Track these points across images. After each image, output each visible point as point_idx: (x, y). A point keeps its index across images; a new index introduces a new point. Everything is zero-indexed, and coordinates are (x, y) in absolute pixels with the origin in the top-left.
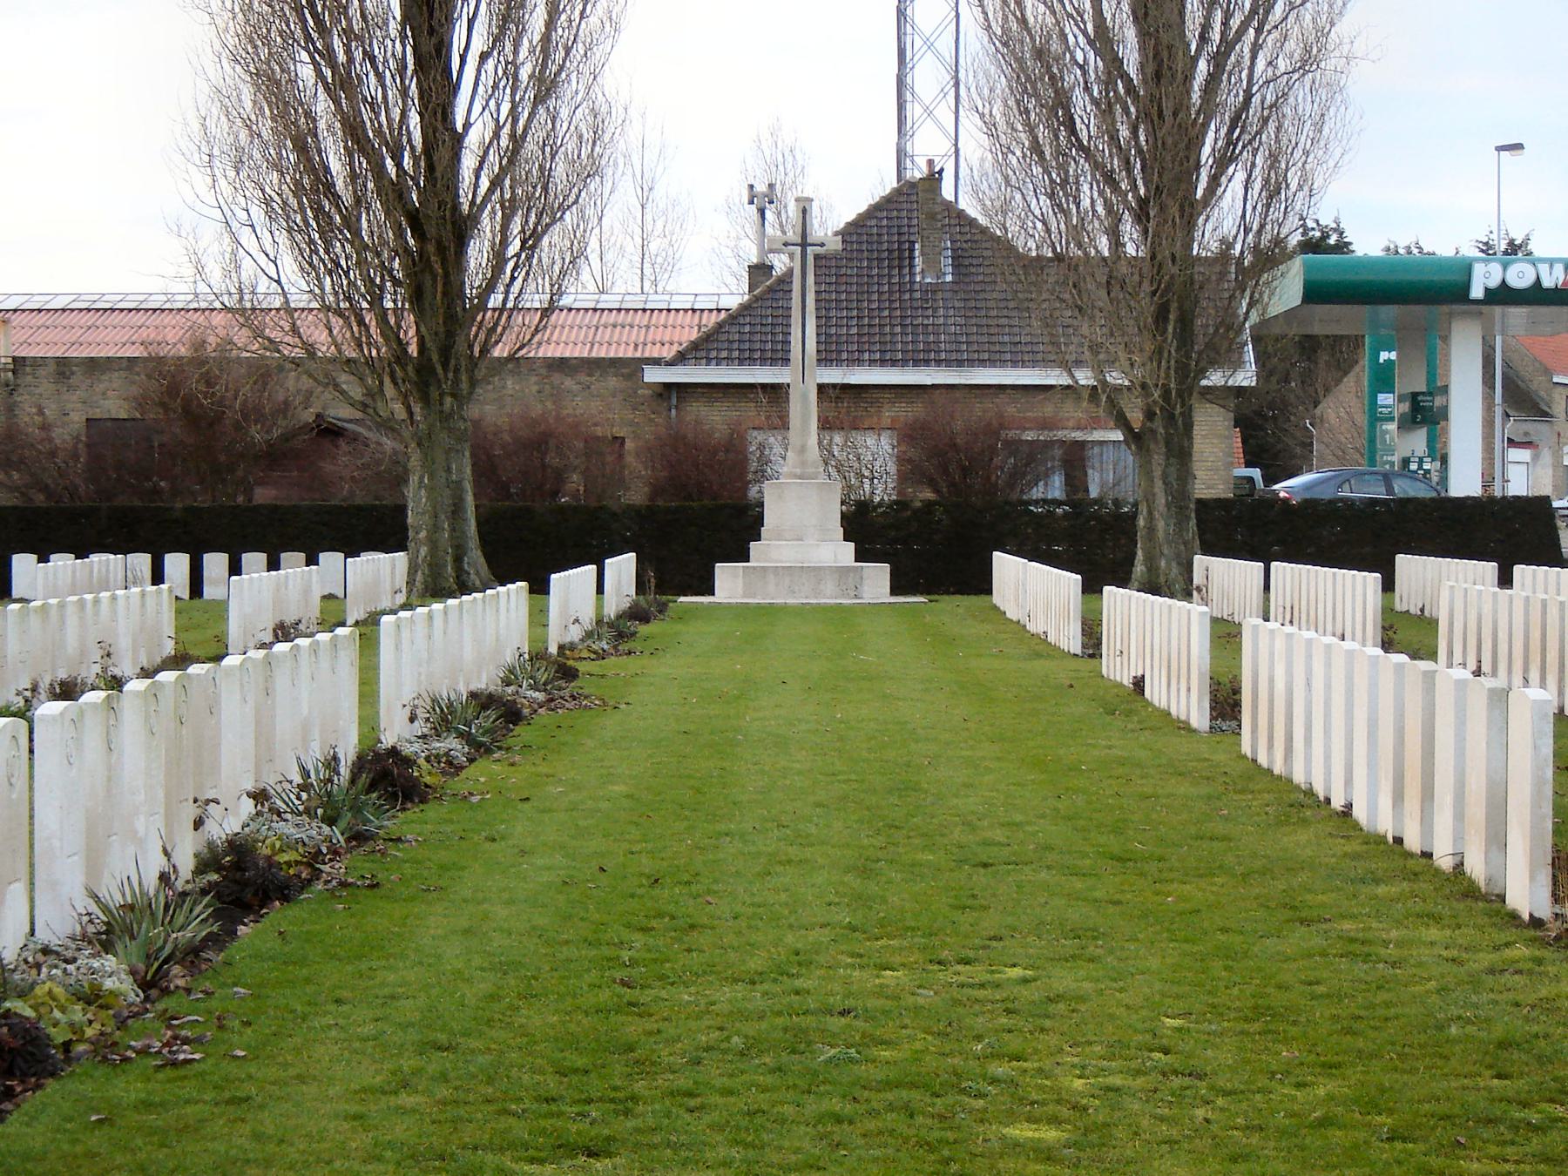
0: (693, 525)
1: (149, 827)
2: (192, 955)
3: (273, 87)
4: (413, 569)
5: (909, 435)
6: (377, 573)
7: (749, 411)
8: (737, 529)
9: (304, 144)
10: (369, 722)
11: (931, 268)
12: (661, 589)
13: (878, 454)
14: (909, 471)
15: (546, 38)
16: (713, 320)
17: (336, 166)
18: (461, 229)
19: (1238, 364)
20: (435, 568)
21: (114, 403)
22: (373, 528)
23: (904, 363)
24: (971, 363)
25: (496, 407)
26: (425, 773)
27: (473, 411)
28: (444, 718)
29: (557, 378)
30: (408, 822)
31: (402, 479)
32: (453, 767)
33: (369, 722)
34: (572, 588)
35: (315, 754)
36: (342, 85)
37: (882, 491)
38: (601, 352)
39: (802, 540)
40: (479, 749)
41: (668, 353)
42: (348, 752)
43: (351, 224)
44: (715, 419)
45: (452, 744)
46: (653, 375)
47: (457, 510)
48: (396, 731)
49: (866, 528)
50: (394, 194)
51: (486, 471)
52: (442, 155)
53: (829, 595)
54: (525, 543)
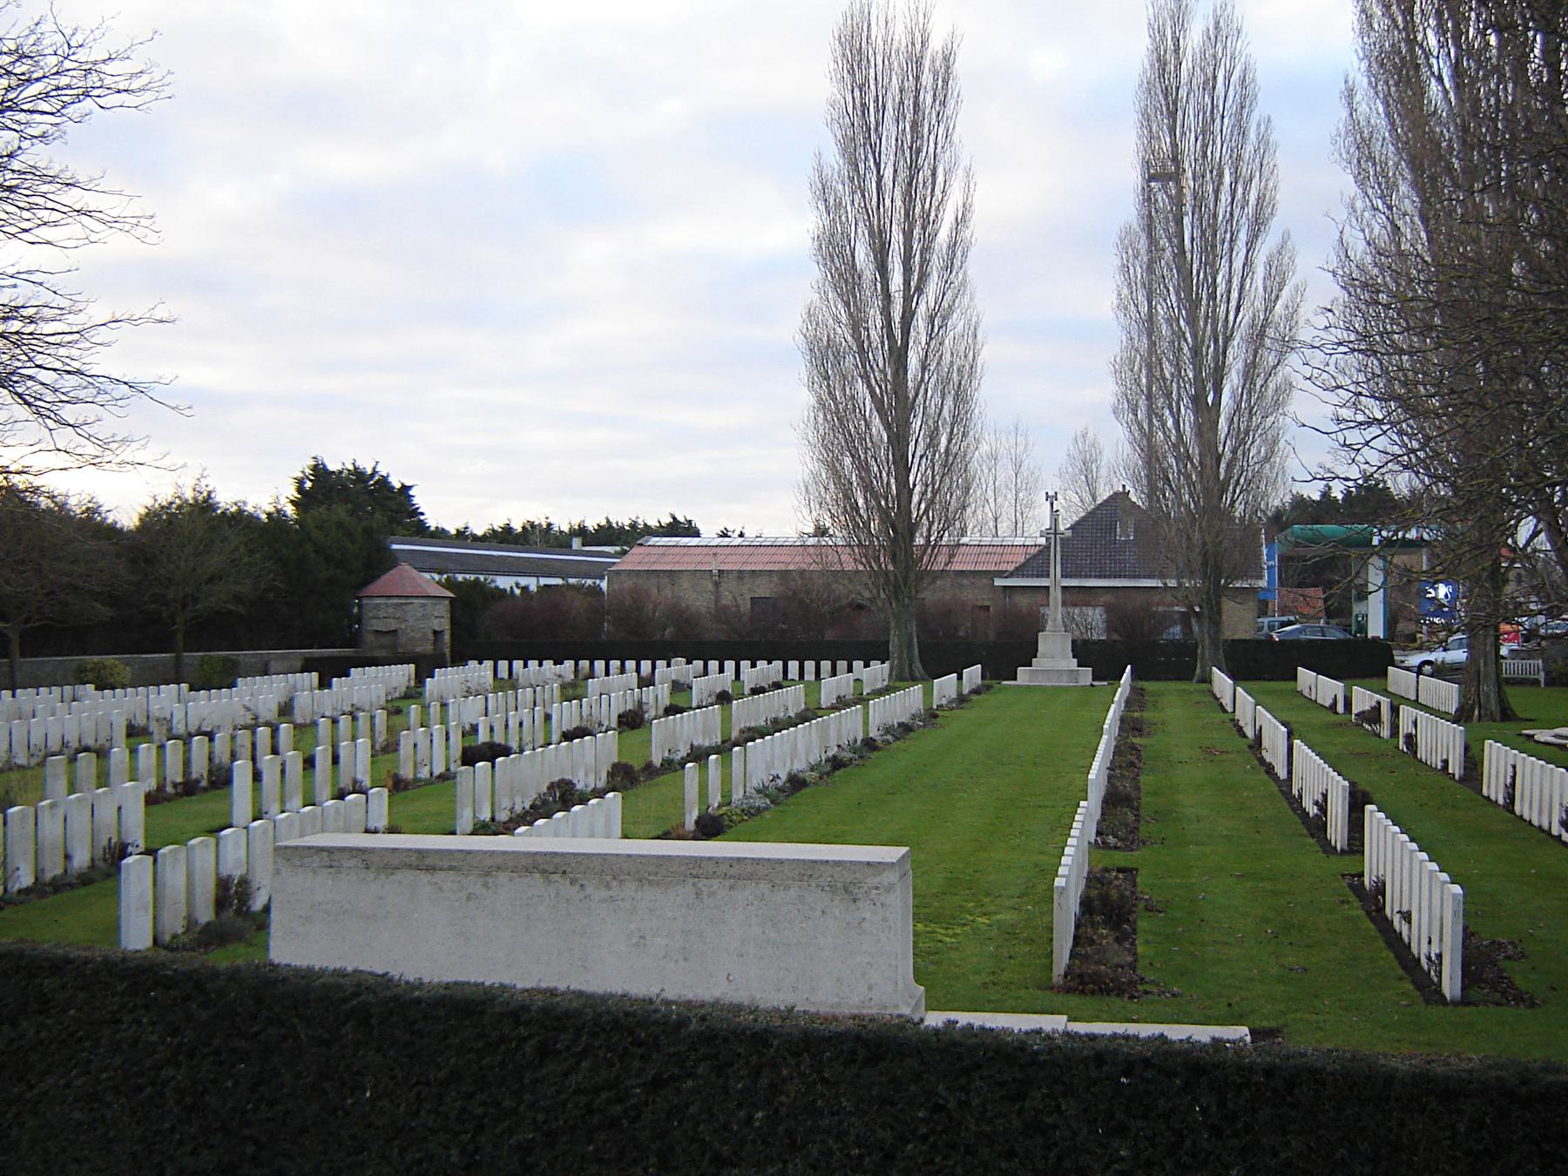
0: (1008, 649)
1: (816, 751)
2: (828, 774)
3: (834, 468)
4: (891, 669)
5: (1109, 609)
6: (876, 673)
7: (1039, 597)
8: (1028, 654)
9: (848, 495)
10: (866, 731)
11: (1125, 533)
12: (992, 678)
13: (1095, 619)
14: (1110, 627)
15: (947, 450)
16: (1033, 551)
17: (861, 502)
18: (912, 529)
19: (1261, 577)
20: (901, 669)
21: (764, 590)
22: (872, 652)
23: (1110, 577)
24: (1139, 577)
25: (931, 595)
26: (879, 743)
27: (920, 596)
28: (888, 730)
29: (959, 580)
30: (875, 755)
31: (887, 631)
32: (889, 743)
33: (866, 731)
34: (946, 685)
35: (851, 738)
36: (862, 467)
37: (1099, 634)
38: (980, 568)
39: (1054, 658)
40: (897, 739)
41: (1011, 568)
42: (860, 737)
43: (867, 525)
44: (1023, 601)
45: (890, 737)
46: (998, 582)
47: (910, 646)
48: (873, 734)
49: (1083, 652)
50: (885, 513)
51: (923, 622)
52: (904, 497)
53: (1064, 682)
54: (939, 656)
